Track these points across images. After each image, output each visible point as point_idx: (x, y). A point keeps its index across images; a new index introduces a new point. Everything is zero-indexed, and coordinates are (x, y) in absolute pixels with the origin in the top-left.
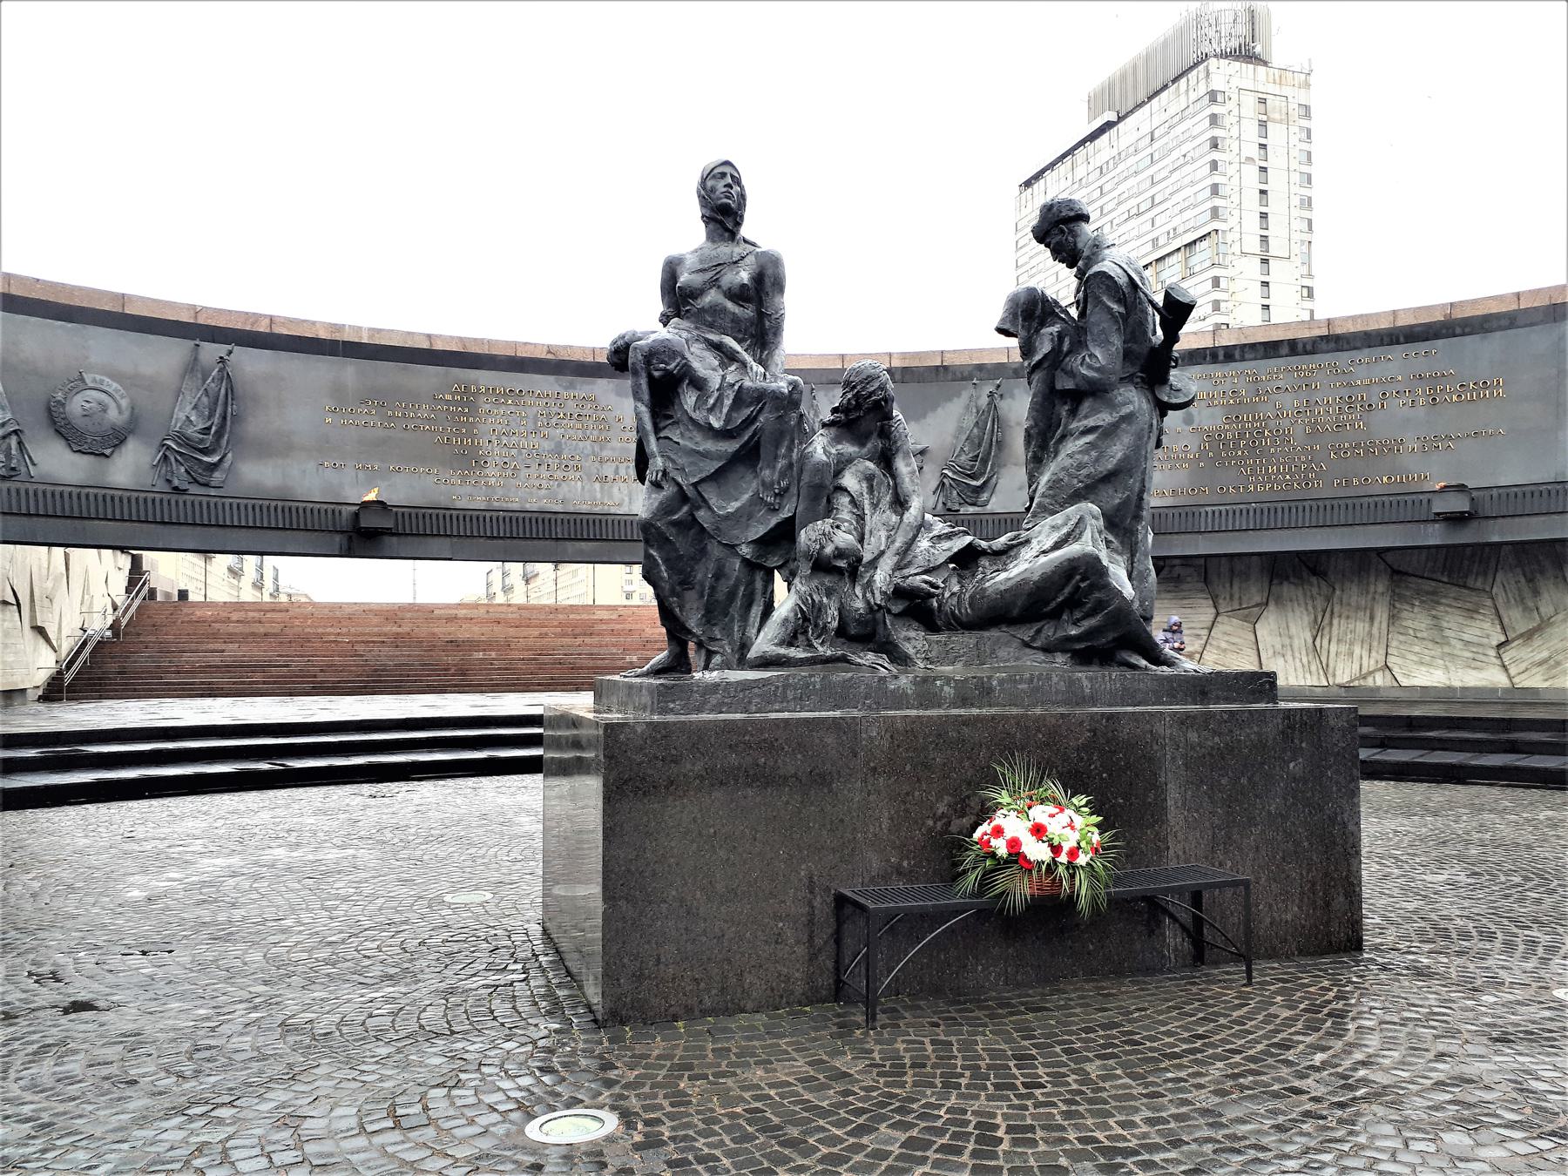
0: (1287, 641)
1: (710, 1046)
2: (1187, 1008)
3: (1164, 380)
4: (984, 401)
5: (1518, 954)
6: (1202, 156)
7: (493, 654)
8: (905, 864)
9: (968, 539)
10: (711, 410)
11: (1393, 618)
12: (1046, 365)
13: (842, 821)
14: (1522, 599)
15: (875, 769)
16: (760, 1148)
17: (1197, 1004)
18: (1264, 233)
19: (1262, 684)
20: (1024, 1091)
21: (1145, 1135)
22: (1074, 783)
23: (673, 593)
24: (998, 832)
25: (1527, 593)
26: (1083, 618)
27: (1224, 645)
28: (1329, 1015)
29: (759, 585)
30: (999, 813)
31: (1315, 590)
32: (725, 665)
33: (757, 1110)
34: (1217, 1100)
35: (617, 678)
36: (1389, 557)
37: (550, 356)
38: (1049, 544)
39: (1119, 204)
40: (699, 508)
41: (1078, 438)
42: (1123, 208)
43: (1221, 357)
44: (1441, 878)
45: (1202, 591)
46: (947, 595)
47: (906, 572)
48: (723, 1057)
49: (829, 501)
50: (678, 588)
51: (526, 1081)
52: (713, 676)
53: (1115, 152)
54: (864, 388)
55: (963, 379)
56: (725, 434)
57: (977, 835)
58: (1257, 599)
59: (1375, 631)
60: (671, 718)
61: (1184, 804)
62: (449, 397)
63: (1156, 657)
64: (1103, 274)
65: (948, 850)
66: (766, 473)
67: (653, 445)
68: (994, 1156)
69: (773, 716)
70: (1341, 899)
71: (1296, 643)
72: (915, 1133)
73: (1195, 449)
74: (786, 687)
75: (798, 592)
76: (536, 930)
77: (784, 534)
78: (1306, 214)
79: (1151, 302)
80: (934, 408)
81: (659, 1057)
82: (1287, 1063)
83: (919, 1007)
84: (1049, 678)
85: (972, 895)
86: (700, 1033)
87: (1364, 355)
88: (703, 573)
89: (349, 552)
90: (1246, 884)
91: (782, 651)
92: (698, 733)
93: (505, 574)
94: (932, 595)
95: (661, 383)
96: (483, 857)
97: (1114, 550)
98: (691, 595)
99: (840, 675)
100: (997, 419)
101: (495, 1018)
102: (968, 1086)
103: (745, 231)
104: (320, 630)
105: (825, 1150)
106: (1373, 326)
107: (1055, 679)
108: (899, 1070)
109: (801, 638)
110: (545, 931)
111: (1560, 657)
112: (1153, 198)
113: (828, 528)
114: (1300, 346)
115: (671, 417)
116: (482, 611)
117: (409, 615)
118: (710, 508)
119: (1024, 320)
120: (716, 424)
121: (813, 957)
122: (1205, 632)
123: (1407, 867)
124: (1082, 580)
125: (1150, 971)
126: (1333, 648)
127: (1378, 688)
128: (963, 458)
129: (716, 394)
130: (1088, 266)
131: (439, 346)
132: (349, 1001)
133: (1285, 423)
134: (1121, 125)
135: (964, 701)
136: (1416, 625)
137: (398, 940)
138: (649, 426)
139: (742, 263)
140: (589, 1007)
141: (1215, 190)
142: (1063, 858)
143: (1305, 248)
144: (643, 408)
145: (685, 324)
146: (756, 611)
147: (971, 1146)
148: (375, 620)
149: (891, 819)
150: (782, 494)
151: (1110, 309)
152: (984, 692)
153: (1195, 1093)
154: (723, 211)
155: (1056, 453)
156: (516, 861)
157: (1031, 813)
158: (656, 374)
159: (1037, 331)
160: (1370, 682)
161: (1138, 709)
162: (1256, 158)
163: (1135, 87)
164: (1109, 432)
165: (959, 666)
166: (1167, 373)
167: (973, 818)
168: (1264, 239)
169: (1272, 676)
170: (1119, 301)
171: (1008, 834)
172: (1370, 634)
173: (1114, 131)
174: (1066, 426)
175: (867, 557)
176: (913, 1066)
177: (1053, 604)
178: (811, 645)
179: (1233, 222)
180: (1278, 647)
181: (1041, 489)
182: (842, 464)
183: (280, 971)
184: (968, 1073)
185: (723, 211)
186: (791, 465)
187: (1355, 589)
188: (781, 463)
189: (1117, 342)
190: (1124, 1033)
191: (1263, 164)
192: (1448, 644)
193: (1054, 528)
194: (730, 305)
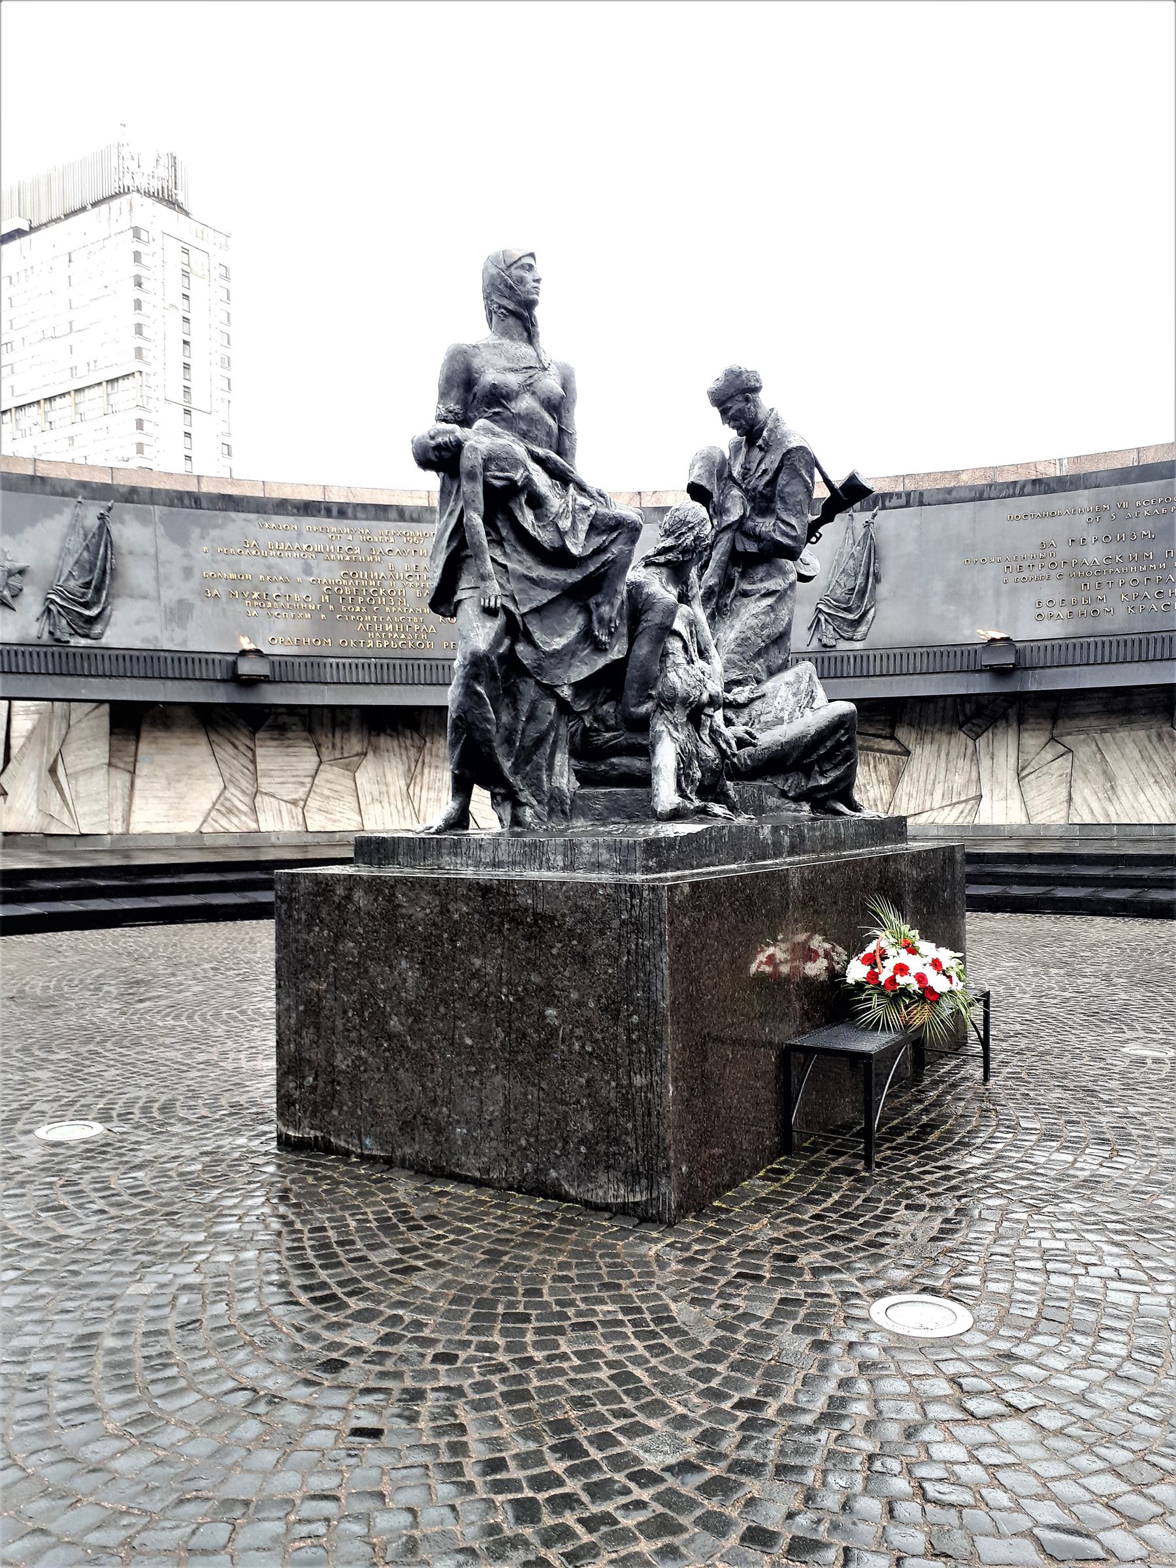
0: (384, 789)
4: (92, 522)
27: (327, 792)
31: (409, 742)
41: (758, 600)
45: (306, 740)
55: (64, 494)
71: (392, 790)
73: (316, 600)
80: (33, 522)
100: (109, 544)
122: (309, 780)
133: (398, 586)
134: (33, 236)
154: (513, 304)
162: (180, 307)
163: (50, 199)
173: (25, 240)
180: (376, 794)
185: (513, 304)
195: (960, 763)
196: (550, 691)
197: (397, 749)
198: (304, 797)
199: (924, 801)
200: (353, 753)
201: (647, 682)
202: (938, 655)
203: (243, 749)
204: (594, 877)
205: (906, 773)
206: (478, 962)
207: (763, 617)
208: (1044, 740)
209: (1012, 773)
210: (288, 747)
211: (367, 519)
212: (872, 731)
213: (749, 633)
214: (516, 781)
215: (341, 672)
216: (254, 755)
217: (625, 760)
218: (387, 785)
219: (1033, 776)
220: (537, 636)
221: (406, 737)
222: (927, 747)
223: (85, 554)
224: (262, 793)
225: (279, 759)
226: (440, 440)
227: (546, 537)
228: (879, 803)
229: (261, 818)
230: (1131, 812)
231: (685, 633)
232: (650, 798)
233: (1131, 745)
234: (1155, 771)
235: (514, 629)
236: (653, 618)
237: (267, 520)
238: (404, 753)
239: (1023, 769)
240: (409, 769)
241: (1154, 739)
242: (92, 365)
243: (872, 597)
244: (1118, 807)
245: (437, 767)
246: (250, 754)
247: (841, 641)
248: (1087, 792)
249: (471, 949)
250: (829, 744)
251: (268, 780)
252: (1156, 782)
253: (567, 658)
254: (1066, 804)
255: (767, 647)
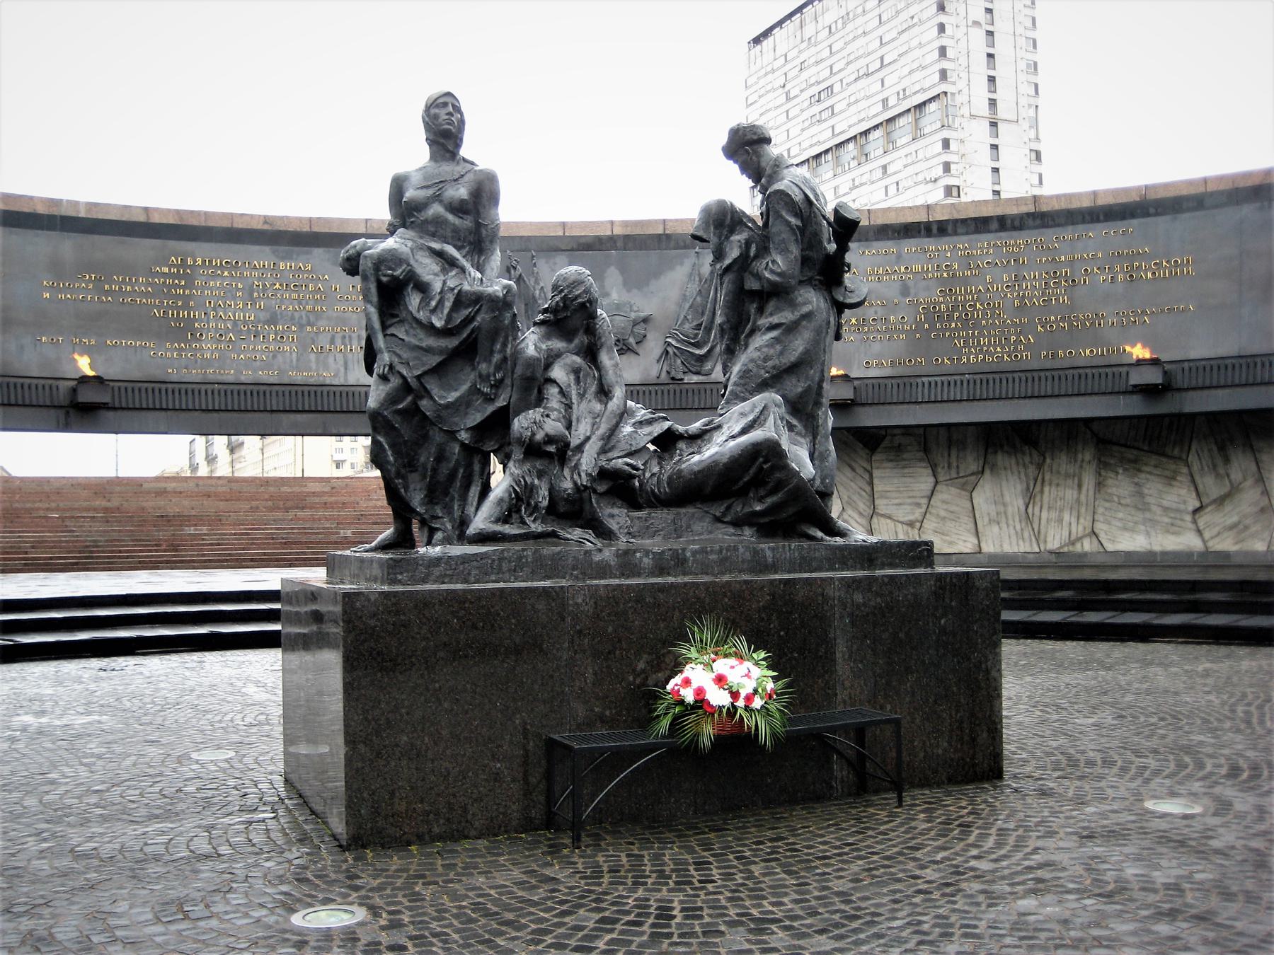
0: (1002, 509)
1: (440, 862)
2: (844, 825)
3: (838, 282)
5: (1128, 776)
6: (929, 19)
7: (205, 530)
8: (607, 713)
9: (667, 424)
10: (433, 311)
11: (1099, 485)
12: (735, 268)
13: (552, 677)
14: (1215, 466)
15: (580, 632)
16: (484, 926)
17: (852, 822)
18: (992, 96)
19: (921, 552)
20: (698, 885)
21: (791, 910)
22: (757, 642)
23: (398, 475)
24: (687, 682)
25: (1219, 461)
26: (767, 495)
28: (960, 825)
29: (477, 467)
30: (688, 667)
31: (1027, 459)
32: (447, 541)
33: (479, 903)
34: (851, 885)
35: (348, 553)
36: (1095, 427)
37: (266, 227)
38: (737, 429)
39: (848, 63)
40: (421, 398)
41: (764, 334)
42: (852, 68)
43: (935, 230)
44: (1090, 721)
45: (921, 460)
46: (648, 475)
47: (610, 455)
48: (451, 870)
49: (540, 392)
50: (403, 471)
51: (284, 888)
52: (436, 551)
53: (843, 12)
54: (570, 292)
56: (446, 332)
57: (669, 687)
58: (974, 467)
59: (1083, 498)
60: (399, 588)
61: (850, 657)
62: (166, 270)
63: (831, 529)
64: (781, 193)
65: (647, 698)
66: (483, 367)
67: (380, 342)
68: (669, 926)
69: (490, 586)
70: (985, 735)
71: (1010, 510)
72: (607, 914)
73: (912, 320)
74: (501, 560)
75: (512, 474)
76: (279, 781)
77: (500, 420)
78: (1033, 79)
79: (824, 217)
81: (397, 871)
82: (915, 859)
83: (619, 832)
84: (736, 549)
85: (663, 737)
86: (431, 854)
87: (1069, 233)
88: (426, 457)
89: (66, 427)
90: (897, 722)
91: (498, 528)
92: (424, 602)
93: (209, 446)
94: (634, 477)
95: (391, 291)
96: (220, 722)
97: (799, 434)
98: (414, 477)
99: (549, 550)
101: (253, 845)
102: (653, 884)
103: (464, 152)
104: (28, 505)
105: (534, 926)
106: (1075, 205)
107: (741, 550)
108: (598, 875)
109: (515, 516)
110: (286, 781)
111: (1248, 522)
112: (882, 58)
113: (538, 417)
114: (1009, 222)
115: (397, 316)
116: (192, 484)
117: (118, 489)
118: (432, 398)
119: (716, 228)
120: (438, 323)
121: (527, 794)
122: (925, 501)
123: (1064, 713)
124: (765, 462)
125: (819, 798)
126: (1044, 515)
127: (1085, 554)
128: (687, 326)
129: (438, 297)
130: (770, 183)
131: (156, 219)
132: (124, 834)
135: (661, 570)
136: (1121, 492)
137: (157, 789)
138: (377, 325)
139: (461, 181)
140: (334, 836)
141: (943, 51)
142: (741, 703)
143: (1032, 112)
144: (373, 310)
145: (410, 233)
146: (474, 491)
147: (651, 920)
148: (85, 494)
149: (595, 674)
150: (498, 385)
151: (788, 223)
152: (678, 562)
153: (836, 881)
154: (444, 131)
155: (746, 346)
156: (251, 725)
157: (714, 665)
158: (384, 279)
159: (727, 238)
160: (1078, 548)
161: (814, 575)
162: (983, 23)
164: (791, 329)
165: (657, 539)
166: (842, 276)
167: (668, 673)
168: (993, 103)
169: (929, 544)
170: (796, 215)
171: (695, 685)
172: (1078, 501)
174: (755, 322)
175: (574, 442)
176: (609, 872)
177: (741, 483)
178: (524, 523)
179: (961, 85)
180: (993, 514)
181: (733, 378)
182: (550, 359)
183: (59, 815)
184: (654, 875)
185: (444, 131)
186: (505, 359)
187: (1064, 457)
188: (496, 358)
189: (795, 251)
190: (787, 844)
191: (990, 28)
192: (1149, 510)
193: (743, 415)
194: (450, 217)
197: (1014, 467)
198: (920, 518)
200: (969, 472)
203: (860, 471)
207: (765, 350)
210: (904, 467)
211: (967, 233)
213: (751, 366)
215: (933, 391)
218: (1005, 505)
221: (1024, 454)
223: (699, 299)
225: (896, 481)
237: (867, 247)
238: (1022, 470)
240: (1028, 488)
242: (902, 95)
245: (1058, 485)
246: (867, 476)
251: (885, 501)
253: (463, 408)
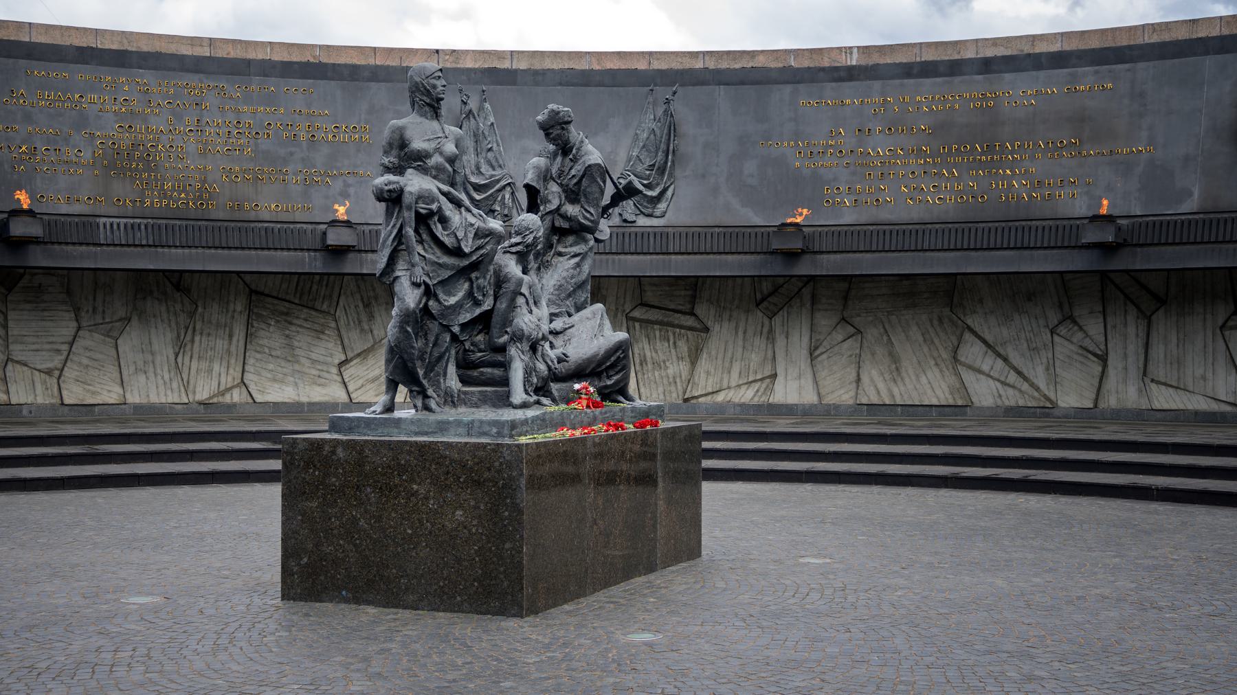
0: (150, 358)
27: (85, 361)
31: (178, 307)
122: (65, 347)
180: (140, 364)
195: (757, 341)
196: (447, 328)
197: (165, 316)
198: (60, 366)
199: (722, 380)
200: (115, 318)
201: (507, 321)
202: (734, 236)
204: (484, 440)
205: (705, 350)
206: (415, 487)
208: (835, 320)
209: (805, 353)
210: (44, 310)
212: (672, 307)
214: (425, 382)
216: (6, 319)
217: (489, 370)
219: (824, 356)
220: (441, 296)
222: (726, 324)
224: (12, 360)
226: (391, 187)
227: (448, 241)
228: (678, 380)
229: (12, 389)
230: (914, 394)
231: (527, 294)
232: (508, 395)
233: (915, 328)
234: (935, 354)
235: (429, 293)
236: (510, 286)
239: (816, 348)
240: (179, 336)
241: (936, 322)
243: (671, 175)
244: (902, 388)
245: (209, 335)
247: (641, 217)
248: (874, 373)
249: (412, 480)
250: (613, 359)
251: (19, 347)
252: (937, 364)
254: (854, 385)
255: (574, 291)
